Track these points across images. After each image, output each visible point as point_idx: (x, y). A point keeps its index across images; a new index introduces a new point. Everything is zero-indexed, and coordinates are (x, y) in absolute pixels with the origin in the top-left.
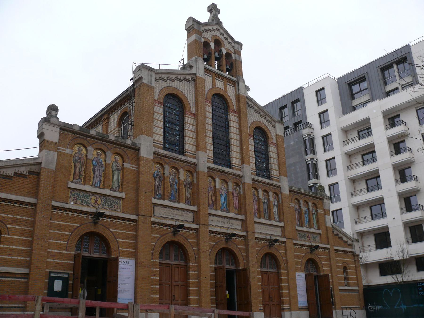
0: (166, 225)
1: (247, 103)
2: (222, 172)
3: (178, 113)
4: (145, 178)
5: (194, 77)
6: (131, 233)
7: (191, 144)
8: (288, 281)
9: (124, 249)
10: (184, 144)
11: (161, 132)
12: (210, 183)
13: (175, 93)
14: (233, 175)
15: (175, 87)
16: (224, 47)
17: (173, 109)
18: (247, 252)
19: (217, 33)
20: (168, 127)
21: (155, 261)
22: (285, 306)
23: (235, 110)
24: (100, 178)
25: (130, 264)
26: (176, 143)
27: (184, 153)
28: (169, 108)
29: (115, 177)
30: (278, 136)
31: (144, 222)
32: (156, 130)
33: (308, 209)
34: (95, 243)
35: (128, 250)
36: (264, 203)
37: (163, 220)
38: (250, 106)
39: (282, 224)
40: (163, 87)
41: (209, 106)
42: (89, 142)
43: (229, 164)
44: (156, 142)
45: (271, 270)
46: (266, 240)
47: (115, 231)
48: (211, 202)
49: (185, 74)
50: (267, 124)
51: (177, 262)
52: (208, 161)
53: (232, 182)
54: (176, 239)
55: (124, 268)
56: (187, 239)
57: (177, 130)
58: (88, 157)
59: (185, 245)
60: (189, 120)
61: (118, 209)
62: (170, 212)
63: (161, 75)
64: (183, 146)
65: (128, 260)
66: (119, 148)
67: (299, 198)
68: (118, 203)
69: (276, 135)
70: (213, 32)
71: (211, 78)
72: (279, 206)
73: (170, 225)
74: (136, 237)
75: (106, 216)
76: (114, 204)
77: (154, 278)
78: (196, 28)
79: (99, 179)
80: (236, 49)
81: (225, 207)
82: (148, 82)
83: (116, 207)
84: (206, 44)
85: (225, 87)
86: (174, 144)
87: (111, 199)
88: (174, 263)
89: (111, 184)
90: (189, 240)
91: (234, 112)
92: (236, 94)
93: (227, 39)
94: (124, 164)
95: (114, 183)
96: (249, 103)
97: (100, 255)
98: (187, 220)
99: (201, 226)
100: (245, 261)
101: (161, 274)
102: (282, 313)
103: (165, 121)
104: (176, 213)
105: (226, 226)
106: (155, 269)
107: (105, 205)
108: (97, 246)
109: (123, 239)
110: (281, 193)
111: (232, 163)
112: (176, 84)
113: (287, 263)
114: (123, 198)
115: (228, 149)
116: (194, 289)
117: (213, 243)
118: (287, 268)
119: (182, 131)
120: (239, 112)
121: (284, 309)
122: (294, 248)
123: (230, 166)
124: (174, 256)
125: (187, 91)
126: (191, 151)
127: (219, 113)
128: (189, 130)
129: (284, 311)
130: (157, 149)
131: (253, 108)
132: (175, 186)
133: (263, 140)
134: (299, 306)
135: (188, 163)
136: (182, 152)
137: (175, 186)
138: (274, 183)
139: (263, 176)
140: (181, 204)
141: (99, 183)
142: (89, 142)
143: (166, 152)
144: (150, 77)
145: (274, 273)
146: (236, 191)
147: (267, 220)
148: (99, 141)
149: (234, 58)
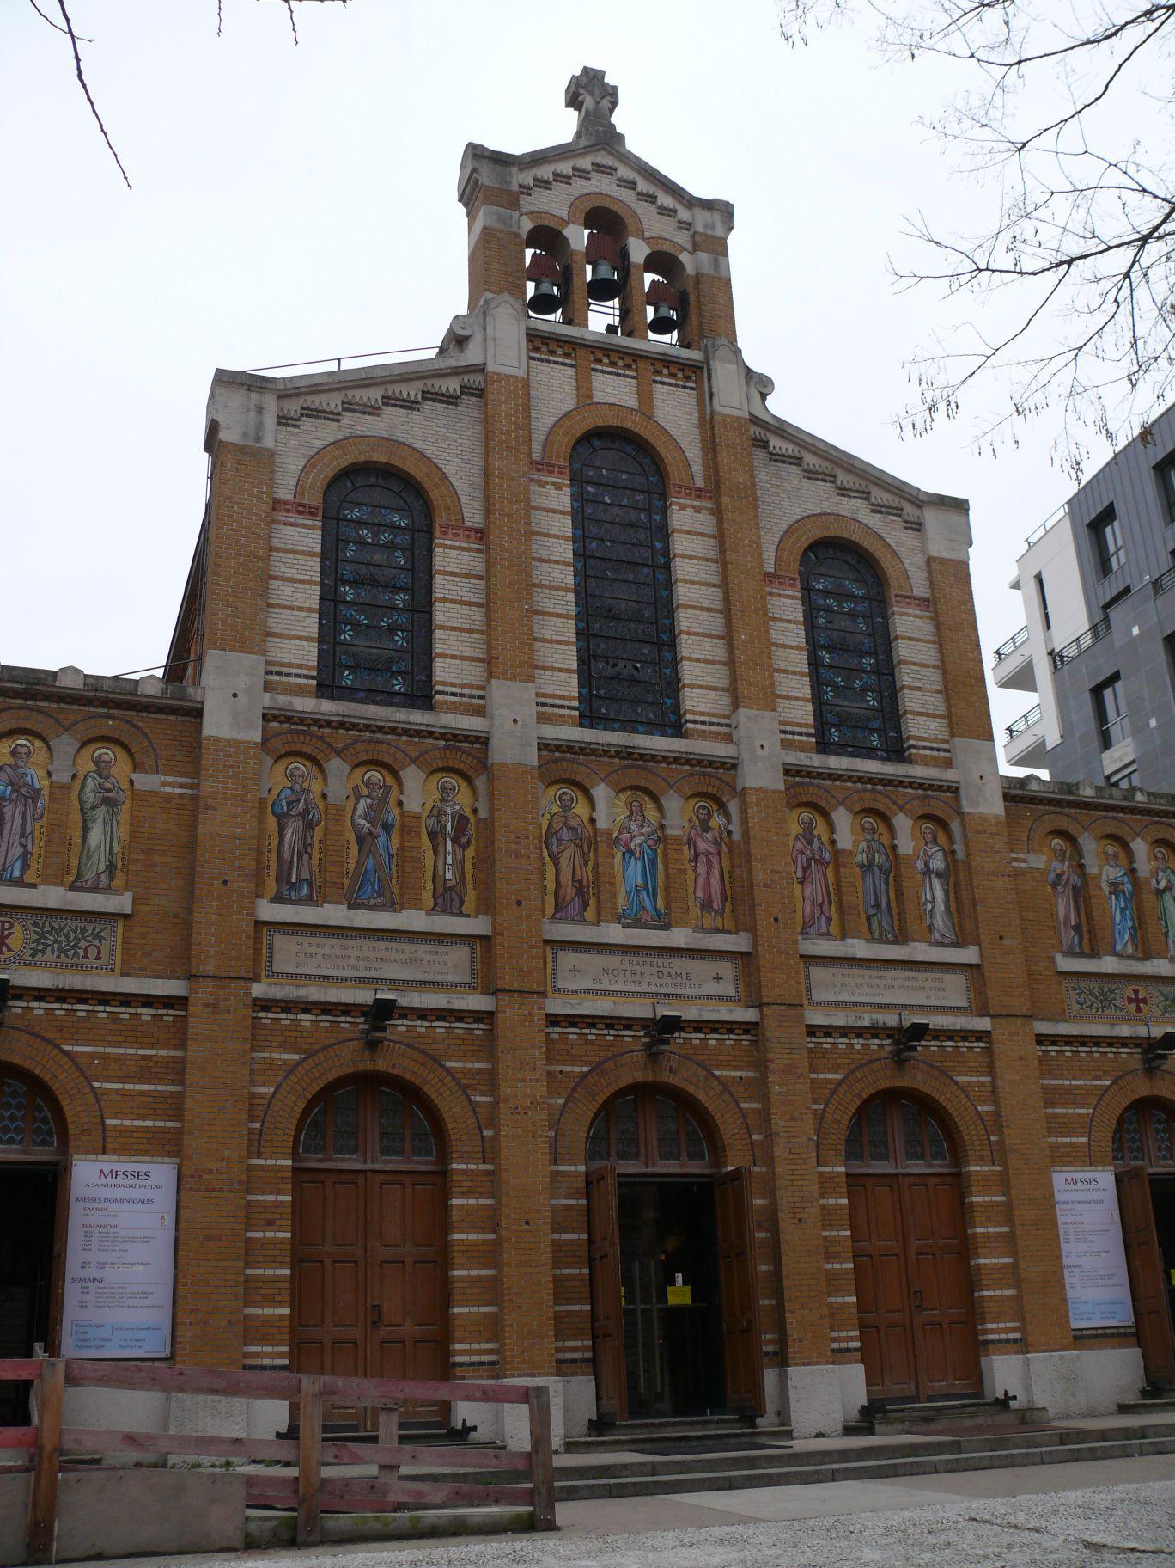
0: (326, 1008)
1: (765, 445)
2: (626, 754)
3: (404, 539)
4: (225, 824)
5: (476, 380)
6: (163, 1053)
7: (462, 658)
8: (1007, 1214)
9: (127, 1123)
10: (899, 717)
11: (803, 687)
12: (566, 808)
13: (384, 459)
15: (384, 433)
16: (640, 233)
17: (843, 596)
18: (765, 1097)
19: (603, 185)
20: (352, 603)
21: (271, 1162)
22: (993, 1331)
23: (700, 483)
24: (24, 846)
25: (1101, 1185)
26: (392, 661)
27: (431, 697)
28: (360, 523)
29: (96, 836)
30: (934, 566)
31: (214, 1006)
32: (280, 620)
33: (1132, 872)
34: (1157, 1131)
35: (149, 1123)
36: (867, 867)
37: (312, 989)
38: (779, 458)
39: (969, 955)
40: (324, 443)
41: (558, 487)
42: (58, 721)
45: (917, 1168)
46: (875, 1031)
47: (89, 1049)
48: (569, 891)
49: (448, 378)
50: (874, 521)
51: (395, 1163)
52: (785, 745)
53: (850, 809)
54: (382, 1064)
55: (122, 1201)
56: (437, 1061)
57: (396, 608)
59: (425, 1089)
60: (452, 560)
61: (104, 960)
62: (354, 953)
63: (309, 399)
64: (898, 728)
65: (143, 1168)
66: (110, 717)
67: (1072, 829)
68: (101, 939)
69: (930, 560)
70: (583, 182)
71: (571, 372)
72: (955, 875)
73: (346, 1009)
74: (177, 1071)
75: (407, 1012)
76: (83, 944)
77: (270, 1234)
78: (487, 182)
79: (20, 850)
80: (700, 229)
81: (648, 904)
82: (245, 435)
83: (92, 952)
84: (547, 237)
85: (645, 398)
86: (385, 668)
87: (69, 925)
88: (376, 1166)
89: (74, 862)
90: (449, 1064)
91: (692, 491)
92: (702, 417)
93: (652, 199)
94: (134, 776)
95: (89, 857)
96: (775, 443)
97: (25, 1152)
98: (440, 978)
99: (505, 999)
100: (755, 1137)
101: (300, 1214)
102: (983, 1360)
103: (813, 645)
104: (382, 954)
105: (651, 989)
106: (271, 1198)
107: (43, 951)
108: (13, 1118)
109: (121, 1080)
110: (961, 815)
111: (908, 738)
112: (391, 424)
113: (999, 1130)
114: (126, 916)
115: (668, 656)
116: (474, 1272)
117: (577, 1069)
118: (998, 1154)
119: (887, 668)
120: (713, 491)
121: (987, 1342)
122: (548, 1039)
123: (677, 728)
124: (661, 1141)
125: (445, 446)
126: (463, 686)
127: (616, 510)
128: (453, 602)
129: (987, 1354)
130: (282, 700)
131: (798, 461)
132: (382, 840)
133: (860, 593)
134: (1074, 1325)
135: (443, 736)
136: (897, 750)
137: (382, 840)
138: (919, 772)
139: (388, 698)
140: (405, 912)
141: (18, 866)
142: (58, 721)
143: (327, 706)
144: (252, 414)
145: (933, 1180)
146: (706, 829)
147: (889, 942)
148: (19, 702)
149: (690, 270)
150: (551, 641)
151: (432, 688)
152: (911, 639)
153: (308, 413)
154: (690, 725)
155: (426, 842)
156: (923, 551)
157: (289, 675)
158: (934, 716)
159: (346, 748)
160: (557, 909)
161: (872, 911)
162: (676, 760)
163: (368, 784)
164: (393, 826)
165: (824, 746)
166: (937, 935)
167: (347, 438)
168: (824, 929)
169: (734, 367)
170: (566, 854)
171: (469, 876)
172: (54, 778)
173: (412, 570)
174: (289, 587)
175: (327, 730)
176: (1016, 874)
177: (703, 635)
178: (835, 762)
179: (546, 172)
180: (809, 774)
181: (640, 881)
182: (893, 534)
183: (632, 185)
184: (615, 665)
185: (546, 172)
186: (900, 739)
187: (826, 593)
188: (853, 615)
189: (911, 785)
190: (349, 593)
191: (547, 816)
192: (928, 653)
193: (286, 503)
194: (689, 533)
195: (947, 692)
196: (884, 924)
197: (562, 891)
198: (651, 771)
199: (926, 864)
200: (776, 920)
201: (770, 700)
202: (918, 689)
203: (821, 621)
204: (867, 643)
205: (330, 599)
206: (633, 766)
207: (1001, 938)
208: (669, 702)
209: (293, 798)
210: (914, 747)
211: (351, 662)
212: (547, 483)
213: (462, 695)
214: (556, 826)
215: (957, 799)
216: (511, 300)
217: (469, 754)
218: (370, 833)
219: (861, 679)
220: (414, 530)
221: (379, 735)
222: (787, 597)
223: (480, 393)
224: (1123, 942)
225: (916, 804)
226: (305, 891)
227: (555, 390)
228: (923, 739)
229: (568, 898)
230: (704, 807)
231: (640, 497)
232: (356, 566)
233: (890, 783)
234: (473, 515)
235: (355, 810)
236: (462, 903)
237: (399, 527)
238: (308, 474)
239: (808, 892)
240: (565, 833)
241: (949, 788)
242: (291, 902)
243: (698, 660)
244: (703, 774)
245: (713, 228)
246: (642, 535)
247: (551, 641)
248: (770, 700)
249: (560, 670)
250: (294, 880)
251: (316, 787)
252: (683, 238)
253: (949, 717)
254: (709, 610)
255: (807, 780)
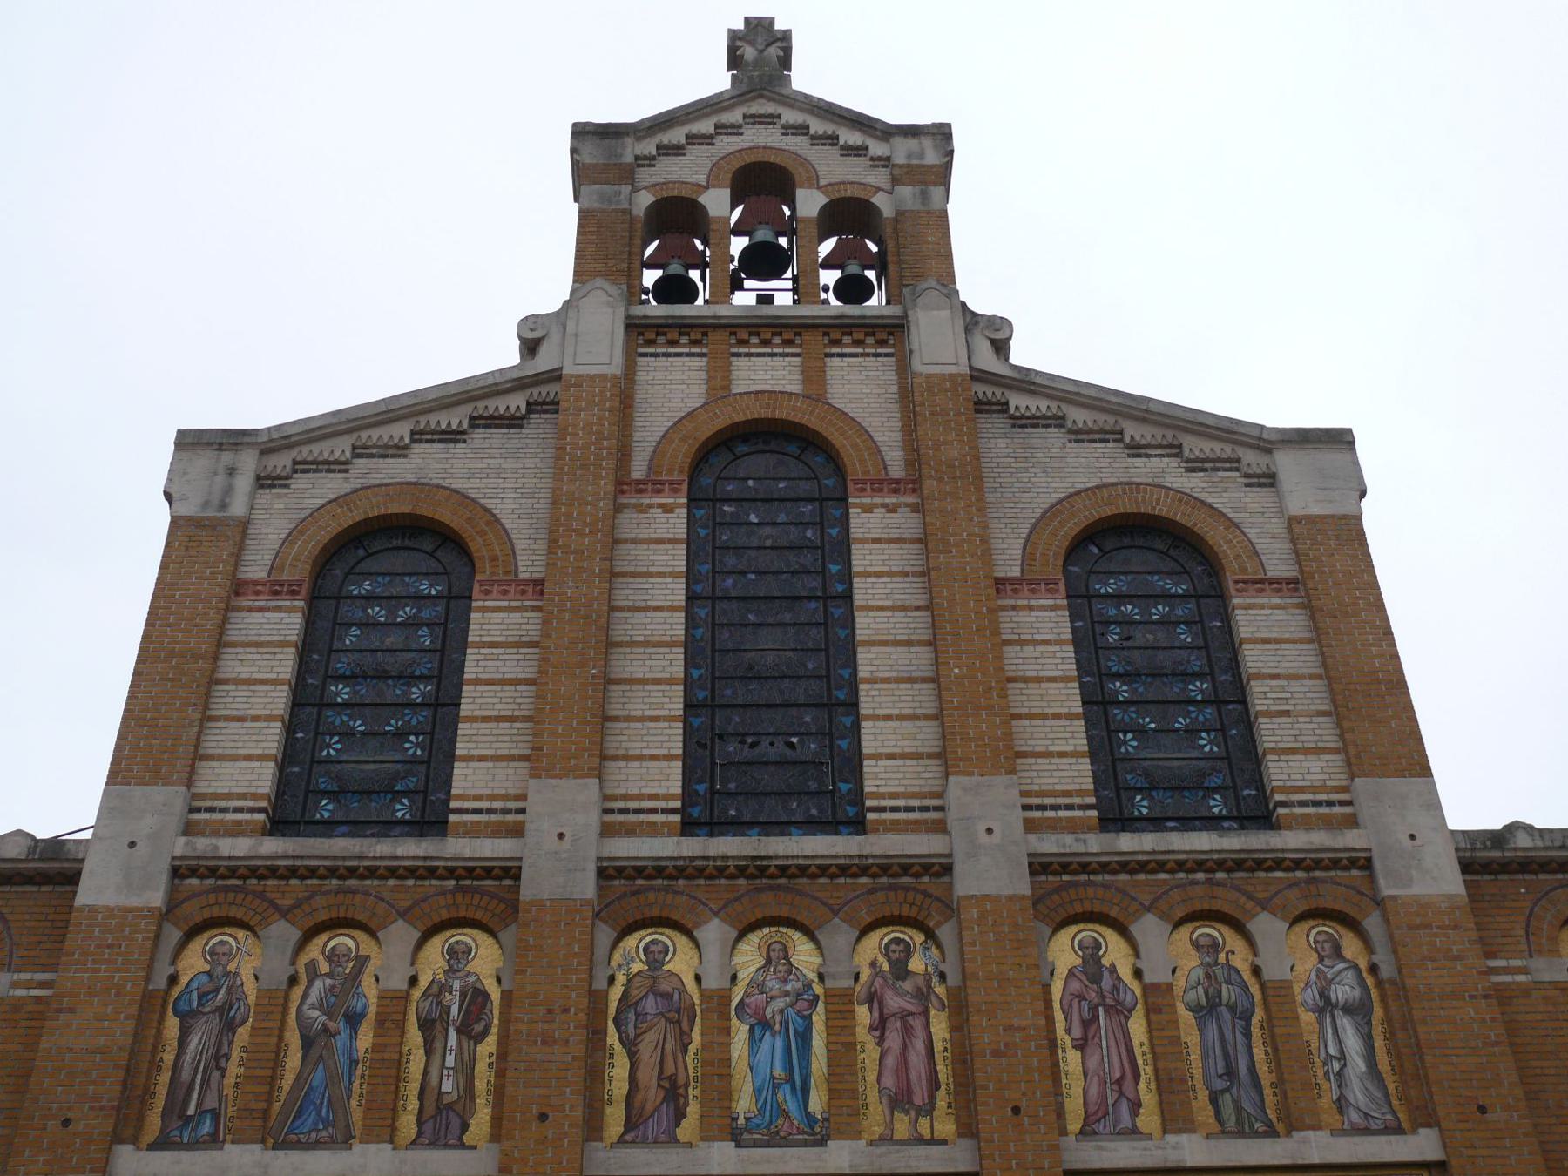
2: (755, 869)
13: (406, 509)
14: (864, 871)
15: (411, 478)
20: (1128, 703)
26: (396, 777)
27: (1270, 814)
30: (1297, 529)
32: (1034, 736)
40: (323, 501)
41: (667, 509)
43: (851, 811)
44: (217, 804)
48: (652, 1094)
50: (1194, 484)
57: (1193, 702)
58: (1267, 974)
64: (1258, 780)
71: (701, 363)
81: (792, 1106)
82: (206, 504)
85: (815, 379)
93: (832, 139)
110: (1379, 903)
123: (1261, 816)
125: (503, 485)
126: (492, 798)
127: (767, 530)
130: (202, 844)
135: (451, 872)
138: (1291, 841)
139: (387, 827)
143: (692, 847)
144: (220, 479)
150: (642, 719)
151: (1266, 800)
152: (1265, 641)
153: (300, 467)
154: (1281, 810)
155: (414, 1036)
156: (1281, 512)
157: (224, 810)
158: (1318, 751)
159: (298, 905)
160: (630, 1125)
161: (1219, 1084)
162: (844, 870)
163: (332, 957)
164: (363, 1015)
165: (1114, 819)
166: (1354, 1116)
167: (356, 491)
168: (1126, 1121)
169: (946, 313)
170: (651, 1037)
171: (481, 1085)
172: (829, 983)
173: (1206, 647)
174: (242, 692)
175: (271, 882)
176: (1503, 996)
177: (898, 680)
178: (1128, 843)
179: (677, 135)
180: (1085, 868)
181: (778, 1071)
182: (1227, 496)
183: (803, 129)
184: (753, 745)
185: (677, 135)
186: (1263, 796)
187: (1119, 598)
188: (1167, 623)
189: (1278, 864)
190: (1123, 691)
191: (621, 979)
192: (1301, 659)
193: (256, 583)
194: (876, 541)
195: (1339, 711)
196: (1246, 1105)
197: (639, 1097)
198: (800, 893)
199: (1323, 994)
200: (1016, 1110)
201: (1008, 758)
202: (1287, 713)
203: (1112, 639)
204: (1196, 662)
205: (1096, 705)
206: (771, 888)
207: (1482, 1109)
208: (844, 787)
209: (210, 987)
210: (1283, 804)
211: (1141, 782)
212: (651, 506)
213: (490, 811)
214: (636, 993)
215: (1372, 879)
216: (607, 286)
217: (493, 896)
218: (325, 1029)
219: (1187, 715)
220: (1198, 597)
221: (352, 882)
222: (1042, 608)
223: (551, 406)
224: (1149, 1119)
225: (1293, 894)
226: (207, 1127)
227: (674, 390)
228: (1301, 790)
229: (649, 1107)
230: (897, 941)
231: (806, 509)
232: (356, 656)
233: (1239, 865)
234: (530, 563)
235: (305, 996)
236: (465, 1127)
237: (1176, 596)
238: (293, 543)
239: (1093, 1063)
240: (650, 1005)
241: (1353, 863)
242: (190, 1146)
243: (888, 718)
244: (892, 888)
245: (922, 155)
246: (807, 559)
247: (642, 719)
248: (1008, 758)
249: (654, 758)
250: (191, 1111)
251: (1241, 961)
252: (879, 177)
253: (1343, 750)
254: (909, 643)
255: (1083, 877)
